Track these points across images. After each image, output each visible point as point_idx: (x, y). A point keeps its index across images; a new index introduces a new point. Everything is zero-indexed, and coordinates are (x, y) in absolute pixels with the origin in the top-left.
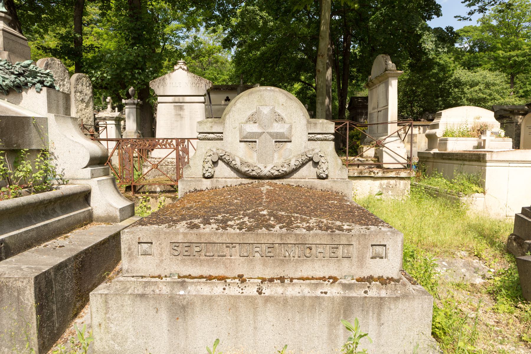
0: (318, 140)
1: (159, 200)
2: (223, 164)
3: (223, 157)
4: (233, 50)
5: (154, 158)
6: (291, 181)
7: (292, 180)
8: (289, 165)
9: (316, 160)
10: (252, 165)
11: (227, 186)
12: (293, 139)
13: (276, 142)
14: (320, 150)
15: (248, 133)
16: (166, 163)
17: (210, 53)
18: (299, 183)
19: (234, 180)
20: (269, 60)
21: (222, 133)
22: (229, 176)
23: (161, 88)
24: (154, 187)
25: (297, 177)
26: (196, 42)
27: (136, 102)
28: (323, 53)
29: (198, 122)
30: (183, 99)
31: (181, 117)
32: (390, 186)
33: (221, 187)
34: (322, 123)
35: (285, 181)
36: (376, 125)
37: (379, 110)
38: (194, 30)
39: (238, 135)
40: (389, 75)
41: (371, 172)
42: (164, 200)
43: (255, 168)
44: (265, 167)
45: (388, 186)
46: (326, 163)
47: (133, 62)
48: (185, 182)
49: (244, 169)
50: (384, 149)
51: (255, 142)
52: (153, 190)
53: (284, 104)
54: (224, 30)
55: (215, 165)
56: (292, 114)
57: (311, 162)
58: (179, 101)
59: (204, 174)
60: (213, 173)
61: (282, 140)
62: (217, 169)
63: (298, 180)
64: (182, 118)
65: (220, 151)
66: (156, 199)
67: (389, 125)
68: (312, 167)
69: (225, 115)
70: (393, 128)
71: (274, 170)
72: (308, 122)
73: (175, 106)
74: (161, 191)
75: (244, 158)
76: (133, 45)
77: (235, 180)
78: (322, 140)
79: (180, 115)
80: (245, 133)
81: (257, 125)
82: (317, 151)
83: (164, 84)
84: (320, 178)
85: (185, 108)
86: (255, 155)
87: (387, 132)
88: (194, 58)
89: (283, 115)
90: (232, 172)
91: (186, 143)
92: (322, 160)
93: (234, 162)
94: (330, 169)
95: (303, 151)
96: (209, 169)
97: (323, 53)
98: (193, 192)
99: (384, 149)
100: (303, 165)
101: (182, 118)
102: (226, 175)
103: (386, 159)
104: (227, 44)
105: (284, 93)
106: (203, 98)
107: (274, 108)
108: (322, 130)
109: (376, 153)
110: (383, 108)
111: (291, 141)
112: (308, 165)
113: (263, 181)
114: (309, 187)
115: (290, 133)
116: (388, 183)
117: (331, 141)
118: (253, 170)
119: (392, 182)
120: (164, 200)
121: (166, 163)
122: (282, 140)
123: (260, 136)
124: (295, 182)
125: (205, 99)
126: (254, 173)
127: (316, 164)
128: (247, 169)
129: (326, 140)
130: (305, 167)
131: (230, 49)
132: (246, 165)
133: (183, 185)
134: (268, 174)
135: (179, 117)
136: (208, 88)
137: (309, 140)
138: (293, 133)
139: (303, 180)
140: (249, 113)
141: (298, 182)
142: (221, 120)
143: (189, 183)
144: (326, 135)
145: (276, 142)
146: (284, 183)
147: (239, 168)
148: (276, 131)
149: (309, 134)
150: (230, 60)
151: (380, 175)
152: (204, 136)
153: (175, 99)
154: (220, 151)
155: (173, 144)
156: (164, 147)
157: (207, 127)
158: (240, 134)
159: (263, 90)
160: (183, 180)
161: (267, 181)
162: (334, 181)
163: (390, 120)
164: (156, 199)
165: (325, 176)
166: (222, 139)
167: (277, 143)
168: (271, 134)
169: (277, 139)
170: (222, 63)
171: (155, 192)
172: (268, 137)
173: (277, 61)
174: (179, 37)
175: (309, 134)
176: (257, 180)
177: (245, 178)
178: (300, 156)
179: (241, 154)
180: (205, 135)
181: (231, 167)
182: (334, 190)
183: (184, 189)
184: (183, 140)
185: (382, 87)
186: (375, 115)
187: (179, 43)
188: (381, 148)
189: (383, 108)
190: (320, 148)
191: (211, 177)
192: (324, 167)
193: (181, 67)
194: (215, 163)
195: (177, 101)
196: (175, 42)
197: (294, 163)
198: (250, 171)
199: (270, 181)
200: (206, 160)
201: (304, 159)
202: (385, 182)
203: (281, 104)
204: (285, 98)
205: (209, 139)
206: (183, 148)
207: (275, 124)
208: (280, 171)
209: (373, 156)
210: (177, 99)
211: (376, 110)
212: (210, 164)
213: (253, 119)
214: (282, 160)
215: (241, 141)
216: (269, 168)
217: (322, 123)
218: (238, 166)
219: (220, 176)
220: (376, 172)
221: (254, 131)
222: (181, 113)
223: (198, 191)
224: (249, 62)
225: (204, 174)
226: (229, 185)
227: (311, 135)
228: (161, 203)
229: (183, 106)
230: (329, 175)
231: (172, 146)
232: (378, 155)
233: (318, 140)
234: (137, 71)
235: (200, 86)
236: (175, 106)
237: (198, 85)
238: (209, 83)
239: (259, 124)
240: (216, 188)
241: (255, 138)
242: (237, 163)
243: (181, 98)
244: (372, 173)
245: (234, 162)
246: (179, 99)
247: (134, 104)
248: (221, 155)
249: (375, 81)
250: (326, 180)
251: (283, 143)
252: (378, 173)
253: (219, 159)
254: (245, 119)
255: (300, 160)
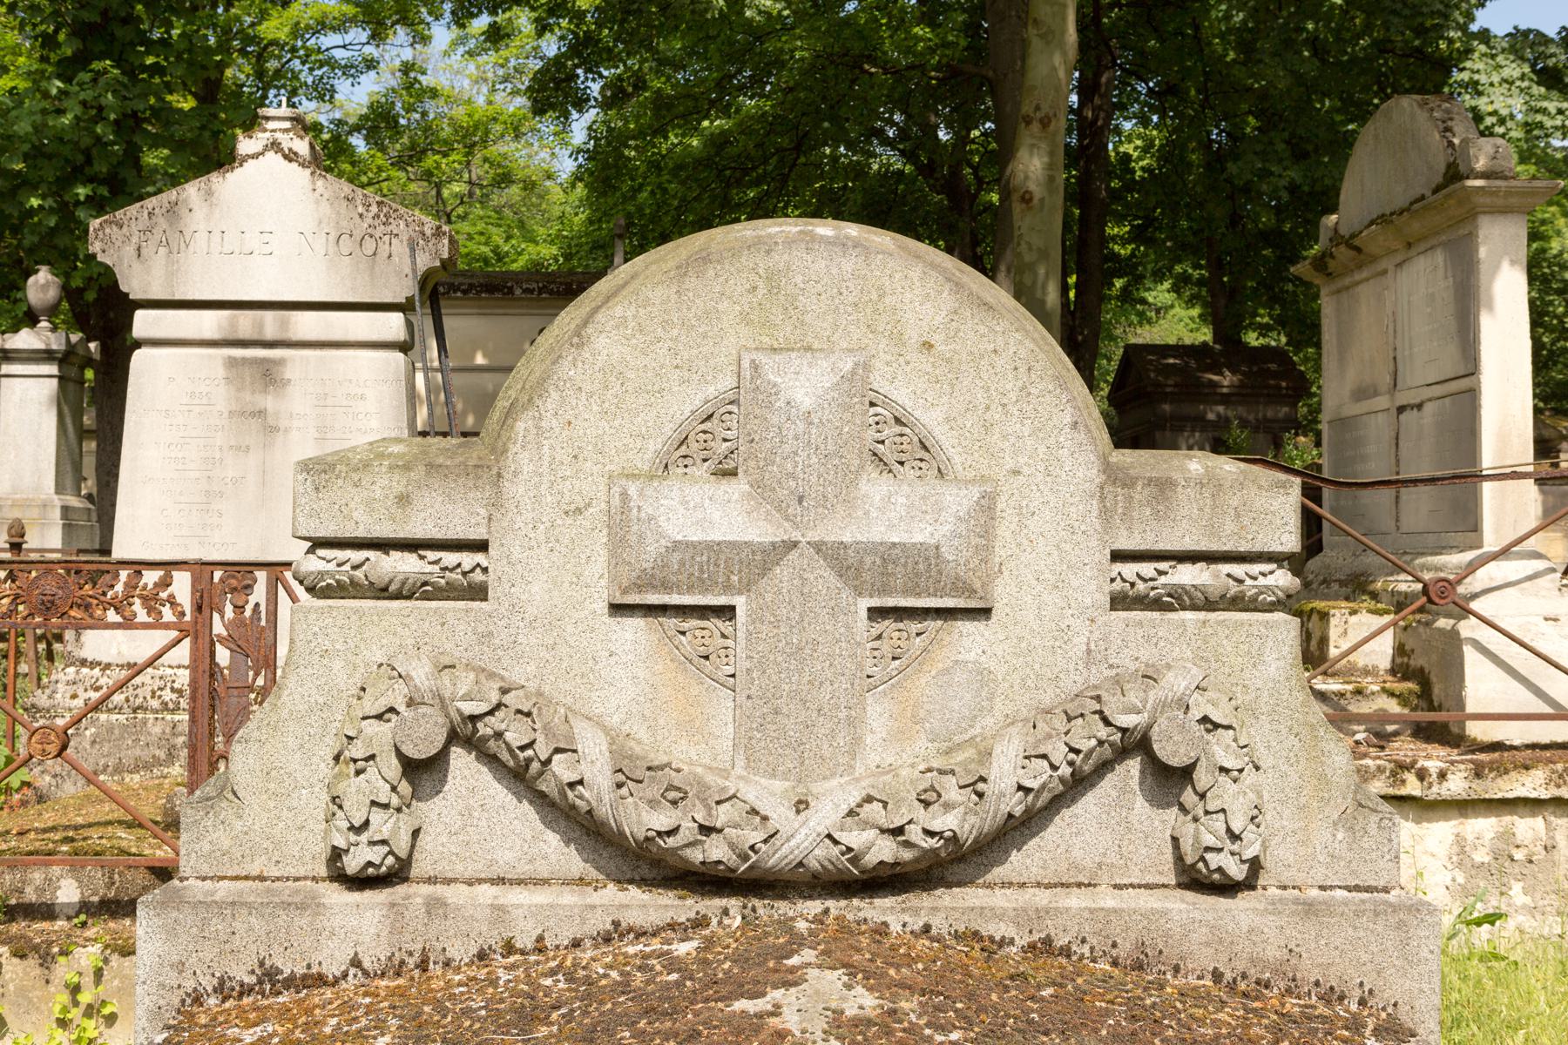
0: (1179, 600)
1: (64, 971)
2: (484, 774)
3: (483, 729)
4: (580, 127)
5: (93, 665)
6: (984, 905)
7: (1001, 899)
8: (976, 786)
9: (1171, 752)
10: (704, 787)
11: (509, 949)
12: (1002, 596)
13: (877, 613)
14: (1197, 674)
15: (676, 545)
16: (168, 695)
17: (473, 137)
18: (1050, 927)
19: (567, 903)
20: (746, 172)
21: (481, 546)
22: (524, 869)
23: (158, 259)
24: (37, 876)
25: (1035, 873)
26: (409, 86)
27: (56, 342)
28: (1045, 109)
29: (306, 467)
30: (284, 324)
31: (268, 427)
32: (1519, 855)
33: (461, 951)
34: (1209, 483)
35: (945, 908)
36: (1387, 494)
37: (1402, 399)
38: (401, 35)
39: (600, 563)
40: (1481, 200)
41: (1402, 767)
42: (98, 974)
43: (722, 815)
44: (801, 805)
45: (1503, 854)
46: (1249, 777)
47: (66, 151)
48: (187, 917)
49: (642, 818)
50: (1468, 628)
51: (727, 612)
52: (30, 896)
53: (937, 339)
54: (542, 28)
55: (426, 783)
56: (996, 414)
57: (1134, 766)
58: (259, 339)
59: (336, 854)
60: (402, 848)
61: (923, 602)
62: (439, 813)
63: (1042, 898)
64: (274, 429)
65: (466, 682)
66: (46, 960)
67: (1487, 487)
68: (1140, 802)
69: (510, 413)
70: (1509, 507)
71: (866, 825)
72: (1113, 475)
73: (232, 363)
74: (84, 907)
75: (643, 734)
76: (80, 61)
77: (569, 897)
78: (1209, 605)
79: (261, 413)
80: (653, 549)
81: (736, 488)
82: (1177, 682)
83: (174, 237)
84: (1197, 879)
85: (289, 373)
86: (722, 709)
87: (1476, 528)
88: (400, 163)
89: (931, 419)
90: (553, 839)
91: (259, 594)
92: (1222, 750)
93: (562, 769)
94: (1268, 817)
95: (1073, 682)
96: (377, 817)
97: (1046, 109)
98: (245, 990)
99: (1468, 628)
100: (1079, 783)
101: (274, 429)
102: (507, 858)
103: (1483, 688)
104: (552, 93)
105: (934, 266)
106: (397, 318)
107: (867, 367)
108: (1212, 530)
109: (1400, 650)
110: (1438, 390)
111: (985, 612)
112: (1108, 785)
113: (783, 907)
114: (1125, 950)
115: (985, 550)
116: (1507, 836)
117: (1270, 608)
118: (706, 830)
119: (1528, 828)
120: (98, 974)
121: (168, 695)
122: (923, 602)
123: (765, 570)
124: (1021, 917)
125: (409, 325)
126: (716, 851)
127: (1169, 781)
128: (660, 820)
129: (1237, 603)
130: (1089, 805)
131: (566, 115)
132: (654, 791)
133: (171, 933)
134: (821, 856)
135: (255, 423)
136: (425, 261)
137: (1119, 602)
138: (1000, 553)
139: (1075, 900)
140: (684, 403)
141: (1041, 913)
142: (476, 450)
143: (217, 925)
144: (1238, 570)
145: (877, 613)
146: (939, 925)
147: (604, 811)
148: (878, 533)
149: (1118, 556)
150: (566, 166)
151: (1457, 785)
152: (356, 567)
153: (233, 324)
154: (466, 682)
155: (171, 601)
156: (112, 617)
157: (369, 504)
158: (613, 554)
159: (790, 242)
160: (179, 901)
161: (814, 907)
162: (1309, 909)
163: (1489, 459)
164: (46, 960)
165: (1237, 871)
166: (478, 592)
167: (888, 625)
168: (839, 559)
169: (884, 591)
170: (529, 186)
171: (47, 912)
172: (823, 578)
173: (785, 179)
174: (331, 63)
175: (1118, 556)
176: (733, 903)
177: (644, 883)
178: (1060, 723)
179: (619, 699)
180: (356, 556)
181: (541, 800)
182: (1309, 972)
183: (180, 967)
184: (241, 571)
185: (1420, 281)
186: (1377, 429)
187: (333, 91)
188: (1443, 623)
189: (1438, 390)
190: (1199, 659)
191: (397, 875)
192: (1233, 799)
193: (275, 146)
194: (422, 772)
195: (245, 332)
196: (315, 86)
197: (1010, 775)
198: (688, 831)
199: (835, 906)
200: (357, 750)
201: (1087, 745)
202: (1483, 827)
203: (913, 336)
204: (947, 300)
205: (382, 592)
206: (239, 622)
207: (874, 487)
208: (914, 834)
209: (1385, 663)
210: (245, 323)
211: (1382, 402)
212: (383, 777)
213: (711, 445)
214: (922, 749)
215: (617, 609)
216: (825, 815)
217: (1209, 483)
218: (599, 792)
219: (459, 869)
220: (1433, 766)
221: (716, 536)
222: (269, 402)
223: (290, 982)
224: (653, 178)
225: (336, 854)
226: (525, 941)
227: (1129, 570)
228: (75, 990)
229: (280, 362)
230: (1267, 862)
231: (168, 615)
232: (1417, 661)
233: (1179, 600)
234: (82, 191)
235: (384, 249)
236: (232, 363)
237: (369, 245)
238: (438, 233)
239: (757, 485)
240: (423, 965)
241: (728, 589)
242: (590, 770)
243: (269, 316)
244: (1411, 778)
245: (562, 769)
246: (260, 326)
247: (46, 356)
248: (469, 708)
249: (1375, 239)
250: (1244, 901)
251: (933, 625)
252: (1442, 775)
253: (453, 737)
254: (654, 445)
255: (1059, 753)
